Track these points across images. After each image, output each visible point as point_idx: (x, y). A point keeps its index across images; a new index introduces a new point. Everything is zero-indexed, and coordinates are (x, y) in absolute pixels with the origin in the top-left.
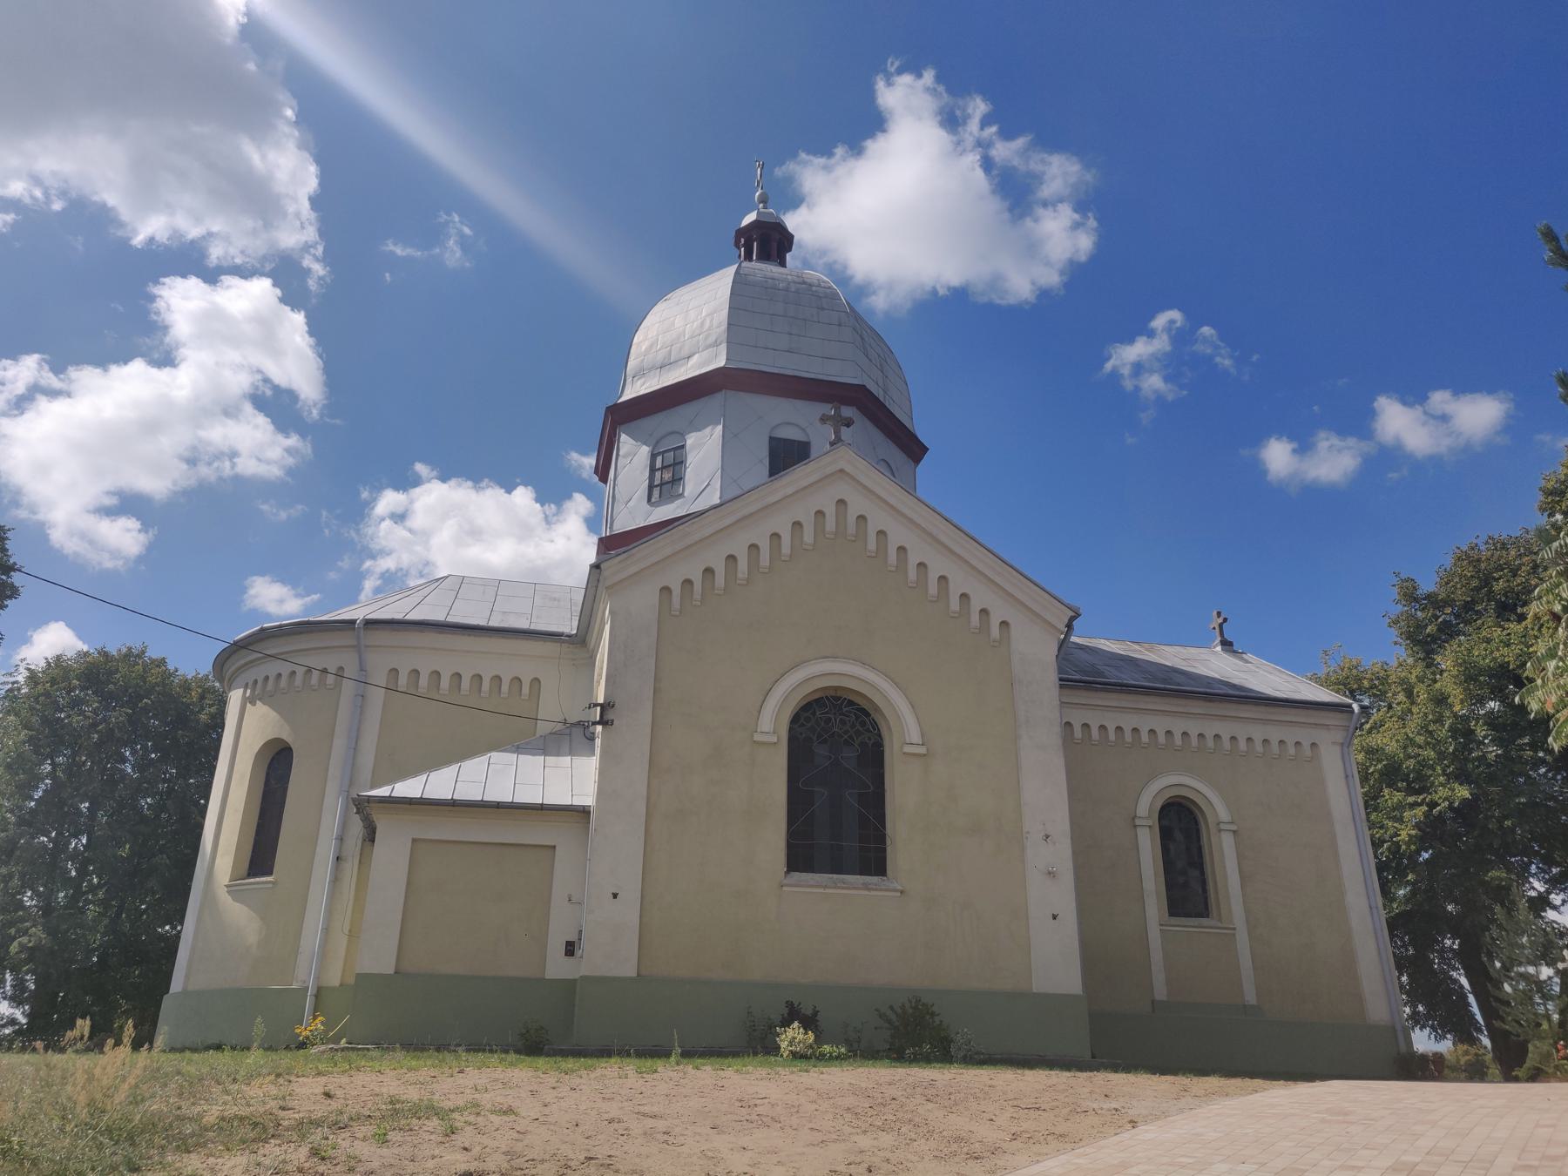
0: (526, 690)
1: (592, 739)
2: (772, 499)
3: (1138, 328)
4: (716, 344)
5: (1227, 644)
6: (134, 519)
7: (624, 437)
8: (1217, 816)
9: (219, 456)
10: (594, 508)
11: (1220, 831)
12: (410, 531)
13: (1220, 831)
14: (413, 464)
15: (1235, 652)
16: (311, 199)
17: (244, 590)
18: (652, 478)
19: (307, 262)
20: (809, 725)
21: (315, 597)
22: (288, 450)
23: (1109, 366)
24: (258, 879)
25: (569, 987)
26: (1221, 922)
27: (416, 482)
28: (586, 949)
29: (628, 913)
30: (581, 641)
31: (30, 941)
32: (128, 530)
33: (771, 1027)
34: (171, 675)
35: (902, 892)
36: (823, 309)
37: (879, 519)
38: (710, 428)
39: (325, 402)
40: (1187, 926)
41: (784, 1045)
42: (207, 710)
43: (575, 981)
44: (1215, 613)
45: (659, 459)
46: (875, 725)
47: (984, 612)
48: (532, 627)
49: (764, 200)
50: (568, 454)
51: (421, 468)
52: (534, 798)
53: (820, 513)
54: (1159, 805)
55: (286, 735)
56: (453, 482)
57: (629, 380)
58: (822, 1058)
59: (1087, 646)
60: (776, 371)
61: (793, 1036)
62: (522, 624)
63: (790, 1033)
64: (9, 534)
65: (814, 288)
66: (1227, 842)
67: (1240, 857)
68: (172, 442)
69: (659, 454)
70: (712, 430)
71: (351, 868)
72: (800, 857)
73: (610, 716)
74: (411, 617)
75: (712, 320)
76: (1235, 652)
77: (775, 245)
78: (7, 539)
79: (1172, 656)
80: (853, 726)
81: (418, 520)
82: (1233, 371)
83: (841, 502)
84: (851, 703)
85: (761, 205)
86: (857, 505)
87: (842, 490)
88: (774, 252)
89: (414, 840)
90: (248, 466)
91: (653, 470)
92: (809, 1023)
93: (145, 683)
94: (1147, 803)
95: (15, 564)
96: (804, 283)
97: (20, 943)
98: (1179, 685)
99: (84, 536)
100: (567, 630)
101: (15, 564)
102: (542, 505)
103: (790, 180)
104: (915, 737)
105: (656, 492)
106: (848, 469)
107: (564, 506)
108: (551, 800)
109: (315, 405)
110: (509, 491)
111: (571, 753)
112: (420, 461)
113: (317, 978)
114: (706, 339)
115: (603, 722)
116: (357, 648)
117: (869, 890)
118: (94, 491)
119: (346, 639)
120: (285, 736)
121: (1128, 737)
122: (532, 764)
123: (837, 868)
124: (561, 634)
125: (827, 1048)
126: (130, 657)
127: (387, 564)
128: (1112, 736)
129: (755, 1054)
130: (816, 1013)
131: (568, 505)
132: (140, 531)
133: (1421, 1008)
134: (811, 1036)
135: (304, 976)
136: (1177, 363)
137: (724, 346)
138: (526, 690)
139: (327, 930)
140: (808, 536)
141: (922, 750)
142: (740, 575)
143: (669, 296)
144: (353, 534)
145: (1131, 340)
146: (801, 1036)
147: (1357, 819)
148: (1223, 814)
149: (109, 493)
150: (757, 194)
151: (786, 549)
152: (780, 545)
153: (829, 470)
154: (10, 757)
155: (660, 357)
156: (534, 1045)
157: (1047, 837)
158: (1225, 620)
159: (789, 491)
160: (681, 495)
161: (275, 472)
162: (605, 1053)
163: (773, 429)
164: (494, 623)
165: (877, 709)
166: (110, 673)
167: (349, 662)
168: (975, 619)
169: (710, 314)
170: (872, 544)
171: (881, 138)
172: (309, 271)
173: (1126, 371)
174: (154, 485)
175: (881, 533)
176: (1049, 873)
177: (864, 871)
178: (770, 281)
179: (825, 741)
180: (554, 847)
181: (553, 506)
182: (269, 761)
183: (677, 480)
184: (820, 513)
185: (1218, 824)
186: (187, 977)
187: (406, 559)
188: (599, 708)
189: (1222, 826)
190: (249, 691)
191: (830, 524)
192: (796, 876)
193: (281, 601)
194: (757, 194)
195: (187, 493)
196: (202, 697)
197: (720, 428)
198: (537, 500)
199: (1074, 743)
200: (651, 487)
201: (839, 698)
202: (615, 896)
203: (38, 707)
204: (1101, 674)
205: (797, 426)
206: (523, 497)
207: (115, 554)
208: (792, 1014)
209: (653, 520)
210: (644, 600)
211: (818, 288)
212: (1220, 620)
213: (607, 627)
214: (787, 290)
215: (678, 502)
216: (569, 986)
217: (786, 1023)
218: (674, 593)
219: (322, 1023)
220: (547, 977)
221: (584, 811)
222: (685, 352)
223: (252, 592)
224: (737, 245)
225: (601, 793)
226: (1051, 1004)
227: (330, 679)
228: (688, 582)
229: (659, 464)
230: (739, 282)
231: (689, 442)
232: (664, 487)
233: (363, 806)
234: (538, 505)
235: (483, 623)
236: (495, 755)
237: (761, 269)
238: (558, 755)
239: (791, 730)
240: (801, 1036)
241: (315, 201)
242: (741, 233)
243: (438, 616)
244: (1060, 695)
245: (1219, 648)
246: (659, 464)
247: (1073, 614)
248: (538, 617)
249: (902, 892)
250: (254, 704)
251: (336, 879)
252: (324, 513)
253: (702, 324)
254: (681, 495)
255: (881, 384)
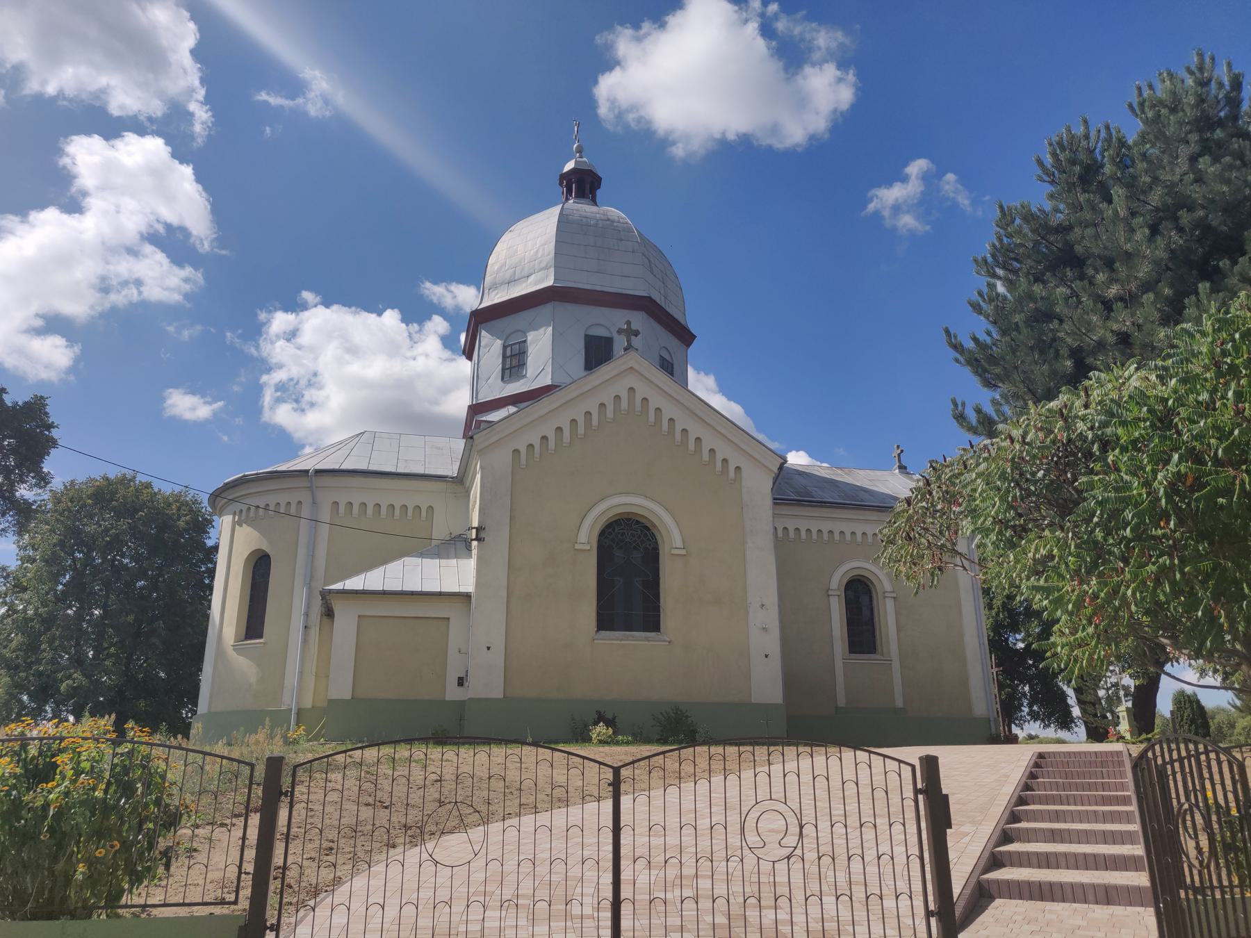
0: (424, 514)
1: (469, 548)
2: (585, 389)
3: (896, 176)
4: (546, 268)
5: (902, 468)
6: (60, 337)
7: (484, 333)
8: (883, 587)
9: (125, 284)
10: (449, 328)
11: (885, 597)
12: (299, 348)
13: (885, 597)
14: (300, 292)
15: (908, 473)
16: (192, 52)
17: (163, 400)
18: (504, 363)
19: (193, 107)
20: (611, 537)
21: (220, 404)
22: (186, 280)
23: (871, 207)
24: (253, 641)
25: (461, 705)
26: (882, 655)
27: (302, 307)
28: (471, 681)
29: (497, 658)
30: (460, 481)
31: (74, 683)
32: (56, 347)
33: (586, 726)
34: (156, 494)
35: (669, 642)
36: (621, 240)
37: (656, 401)
38: (543, 329)
39: (214, 236)
40: (862, 659)
41: (594, 736)
42: (183, 519)
43: (464, 701)
44: (896, 446)
45: (509, 350)
46: (653, 536)
47: (725, 461)
48: (426, 472)
49: (580, 150)
50: (423, 283)
51: (307, 296)
52: (435, 588)
53: (617, 397)
54: (845, 582)
55: (266, 547)
56: (335, 307)
57: (486, 291)
58: (617, 743)
59: (804, 472)
60: (589, 287)
61: (600, 730)
62: (419, 470)
63: (598, 729)
64: (47, 401)
65: (615, 224)
66: (890, 605)
67: (897, 613)
68: (86, 271)
69: (508, 346)
70: (545, 330)
71: (314, 632)
72: (607, 620)
73: (482, 535)
74: (343, 467)
75: (544, 249)
76: (908, 473)
77: (588, 186)
78: (47, 405)
79: (863, 478)
80: (639, 537)
81: (306, 338)
82: (969, 209)
83: (632, 389)
84: (638, 522)
85: (578, 154)
86: (642, 391)
87: (631, 381)
88: (587, 191)
89: (359, 616)
90: (154, 293)
91: (504, 357)
92: (609, 723)
93: (139, 500)
94: (837, 581)
95: (53, 423)
96: (608, 220)
97: (67, 685)
98: (862, 501)
99: (21, 352)
100: (450, 474)
101: (53, 423)
102: (407, 325)
103: (610, 47)
104: (679, 544)
105: (507, 372)
106: (636, 367)
107: (426, 326)
108: (445, 589)
109: (206, 238)
110: (380, 314)
111: (456, 557)
112: (307, 289)
113: (297, 703)
114: (540, 262)
115: (477, 539)
116: (310, 488)
117: (649, 641)
118: (24, 315)
119: (303, 482)
120: (264, 548)
121: (826, 536)
122: (431, 564)
123: (629, 628)
124: (446, 477)
125: (620, 738)
126: (124, 481)
127: (279, 376)
128: (815, 536)
129: (577, 742)
130: (614, 718)
131: (429, 326)
132: (67, 347)
133: (1035, 708)
134: (610, 731)
135: (289, 701)
136: (928, 203)
137: (552, 270)
138: (424, 514)
139: (301, 673)
140: (610, 413)
141: (683, 552)
142: (565, 441)
143: (513, 227)
144: (253, 350)
145: (889, 183)
146: (604, 731)
147: (975, 587)
148: (888, 586)
149: (37, 315)
150: (575, 146)
151: (595, 422)
152: (591, 419)
153: (624, 367)
154: (47, 555)
155: (508, 275)
156: (441, 739)
157: (763, 605)
158: (902, 451)
159: (597, 383)
160: (525, 376)
161: (176, 297)
162: (488, 741)
163: (587, 328)
164: (400, 470)
165: (654, 526)
166: (114, 493)
167: (305, 496)
168: (719, 465)
169: (543, 245)
170: (652, 418)
171: (679, 13)
172: (192, 115)
173: (886, 213)
174: (77, 308)
175: (658, 410)
176: (764, 629)
177: (646, 629)
178: (584, 219)
179: (621, 548)
180: (449, 618)
181: (415, 325)
182: (253, 564)
183: (521, 365)
184: (617, 397)
185: (884, 593)
186: (210, 704)
187: (295, 371)
188: (474, 531)
189: (887, 594)
190: (237, 517)
191: (624, 405)
192: (603, 633)
193: (193, 409)
194: (575, 146)
195: (102, 315)
196: (179, 509)
197: (550, 329)
198: (403, 320)
199: (783, 544)
200: (503, 370)
201: (630, 519)
202: (489, 648)
203: (62, 518)
204: (809, 494)
205: (603, 325)
206: (391, 318)
207: (47, 366)
208: (600, 718)
209: (505, 393)
210: (502, 458)
211: (619, 225)
212: (899, 451)
213: (478, 476)
214: (596, 225)
215: (522, 381)
216: (461, 704)
217: (596, 723)
218: (522, 453)
219: (304, 730)
220: (447, 699)
221: (467, 596)
222: (525, 273)
223: (170, 402)
224: (561, 184)
225: (478, 584)
226: (765, 709)
227: (261, 511)
228: (531, 446)
229: (508, 353)
230: (563, 220)
231: (529, 338)
232: (513, 370)
233: (326, 595)
234: (404, 325)
235: (393, 470)
236: (407, 560)
237: (577, 207)
238: (448, 558)
239: (599, 541)
240: (604, 731)
241: (196, 53)
242: (563, 177)
243: (362, 466)
244: (775, 515)
245: (897, 471)
246: (508, 353)
247: (783, 461)
248: (429, 463)
249: (669, 642)
250: (241, 525)
251: (305, 641)
252: (228, 334)
253: (537, 252)
254: (525, 376)
255: (662, 292)
